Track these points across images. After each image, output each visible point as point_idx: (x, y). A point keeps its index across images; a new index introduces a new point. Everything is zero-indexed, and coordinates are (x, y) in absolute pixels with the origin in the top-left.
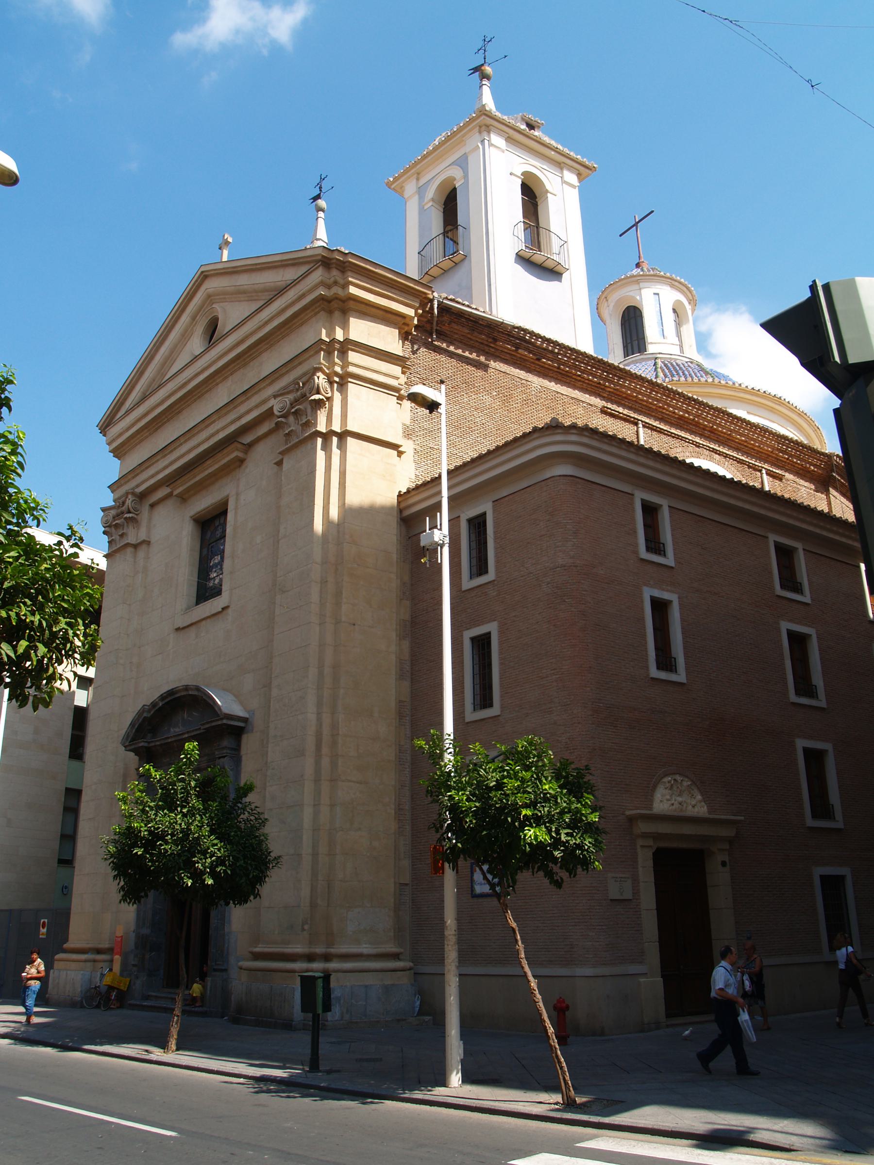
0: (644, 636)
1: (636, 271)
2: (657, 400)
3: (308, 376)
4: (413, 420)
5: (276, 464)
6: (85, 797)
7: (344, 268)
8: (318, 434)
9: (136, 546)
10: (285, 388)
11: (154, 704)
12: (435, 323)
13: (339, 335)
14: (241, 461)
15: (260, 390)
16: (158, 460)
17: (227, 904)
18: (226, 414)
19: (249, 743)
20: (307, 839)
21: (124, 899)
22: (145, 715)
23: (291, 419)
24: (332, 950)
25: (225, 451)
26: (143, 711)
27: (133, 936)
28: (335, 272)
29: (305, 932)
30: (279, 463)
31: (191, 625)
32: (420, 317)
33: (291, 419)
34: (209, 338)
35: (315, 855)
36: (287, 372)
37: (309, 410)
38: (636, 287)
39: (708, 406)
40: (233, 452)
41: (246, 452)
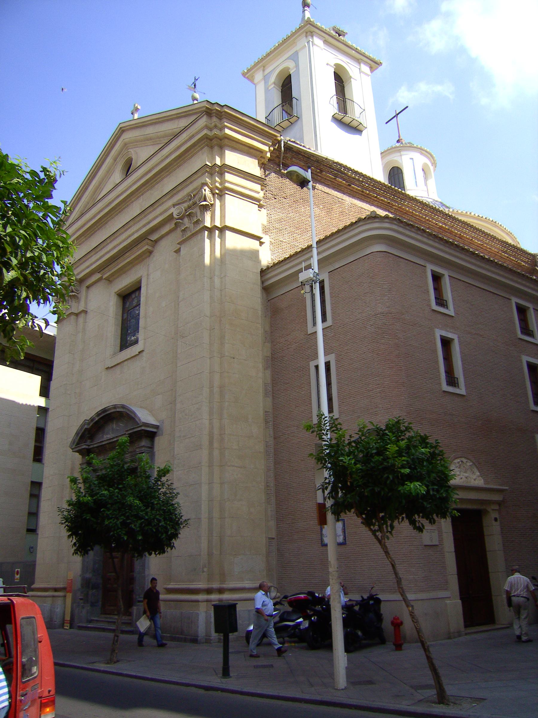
0: (437, 362)
1: (398, 145)
2: (426, 215)
3: (197, 190)
4: (269, 222)
5: (175, 252)
6: (44, 486)
7: (221, 116)
8: (206, 228)
9: (77, 315)
10: (181, 199)
11: (92, 419)
12: (282, 157)
13: (218, 161)
14: (151, 252)
15: (163, 203)
16: (92, 256)
17: (150, 554)
18: (139, 221)
19: (160, 443)
20: (204, 508)
21: (75, 553)
22: (86, 427)
23: (186, 220)
24: (224, 586)
25: (139, 246)
26: (84, 425)
27: (79, 579)
28: (215, 119)
29: (204, 573)
30: (178, 251)
31: (118, 364)
32: (272, 153)
33: (186, 220)
34: (126, 173)
35: (210, 519)
36: (182, 189)
37: (199, 214)
38: (399, 154)
39: (458, 220)
40: (144, 246)
41: (153, 246)
